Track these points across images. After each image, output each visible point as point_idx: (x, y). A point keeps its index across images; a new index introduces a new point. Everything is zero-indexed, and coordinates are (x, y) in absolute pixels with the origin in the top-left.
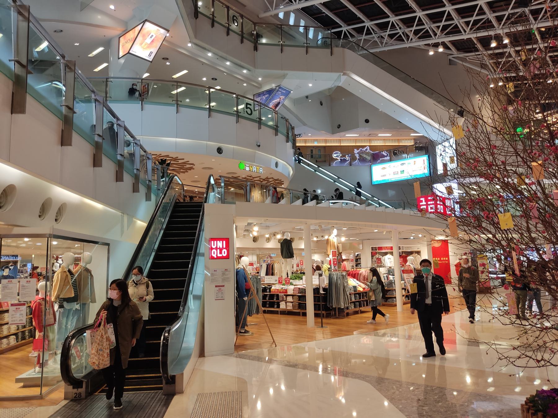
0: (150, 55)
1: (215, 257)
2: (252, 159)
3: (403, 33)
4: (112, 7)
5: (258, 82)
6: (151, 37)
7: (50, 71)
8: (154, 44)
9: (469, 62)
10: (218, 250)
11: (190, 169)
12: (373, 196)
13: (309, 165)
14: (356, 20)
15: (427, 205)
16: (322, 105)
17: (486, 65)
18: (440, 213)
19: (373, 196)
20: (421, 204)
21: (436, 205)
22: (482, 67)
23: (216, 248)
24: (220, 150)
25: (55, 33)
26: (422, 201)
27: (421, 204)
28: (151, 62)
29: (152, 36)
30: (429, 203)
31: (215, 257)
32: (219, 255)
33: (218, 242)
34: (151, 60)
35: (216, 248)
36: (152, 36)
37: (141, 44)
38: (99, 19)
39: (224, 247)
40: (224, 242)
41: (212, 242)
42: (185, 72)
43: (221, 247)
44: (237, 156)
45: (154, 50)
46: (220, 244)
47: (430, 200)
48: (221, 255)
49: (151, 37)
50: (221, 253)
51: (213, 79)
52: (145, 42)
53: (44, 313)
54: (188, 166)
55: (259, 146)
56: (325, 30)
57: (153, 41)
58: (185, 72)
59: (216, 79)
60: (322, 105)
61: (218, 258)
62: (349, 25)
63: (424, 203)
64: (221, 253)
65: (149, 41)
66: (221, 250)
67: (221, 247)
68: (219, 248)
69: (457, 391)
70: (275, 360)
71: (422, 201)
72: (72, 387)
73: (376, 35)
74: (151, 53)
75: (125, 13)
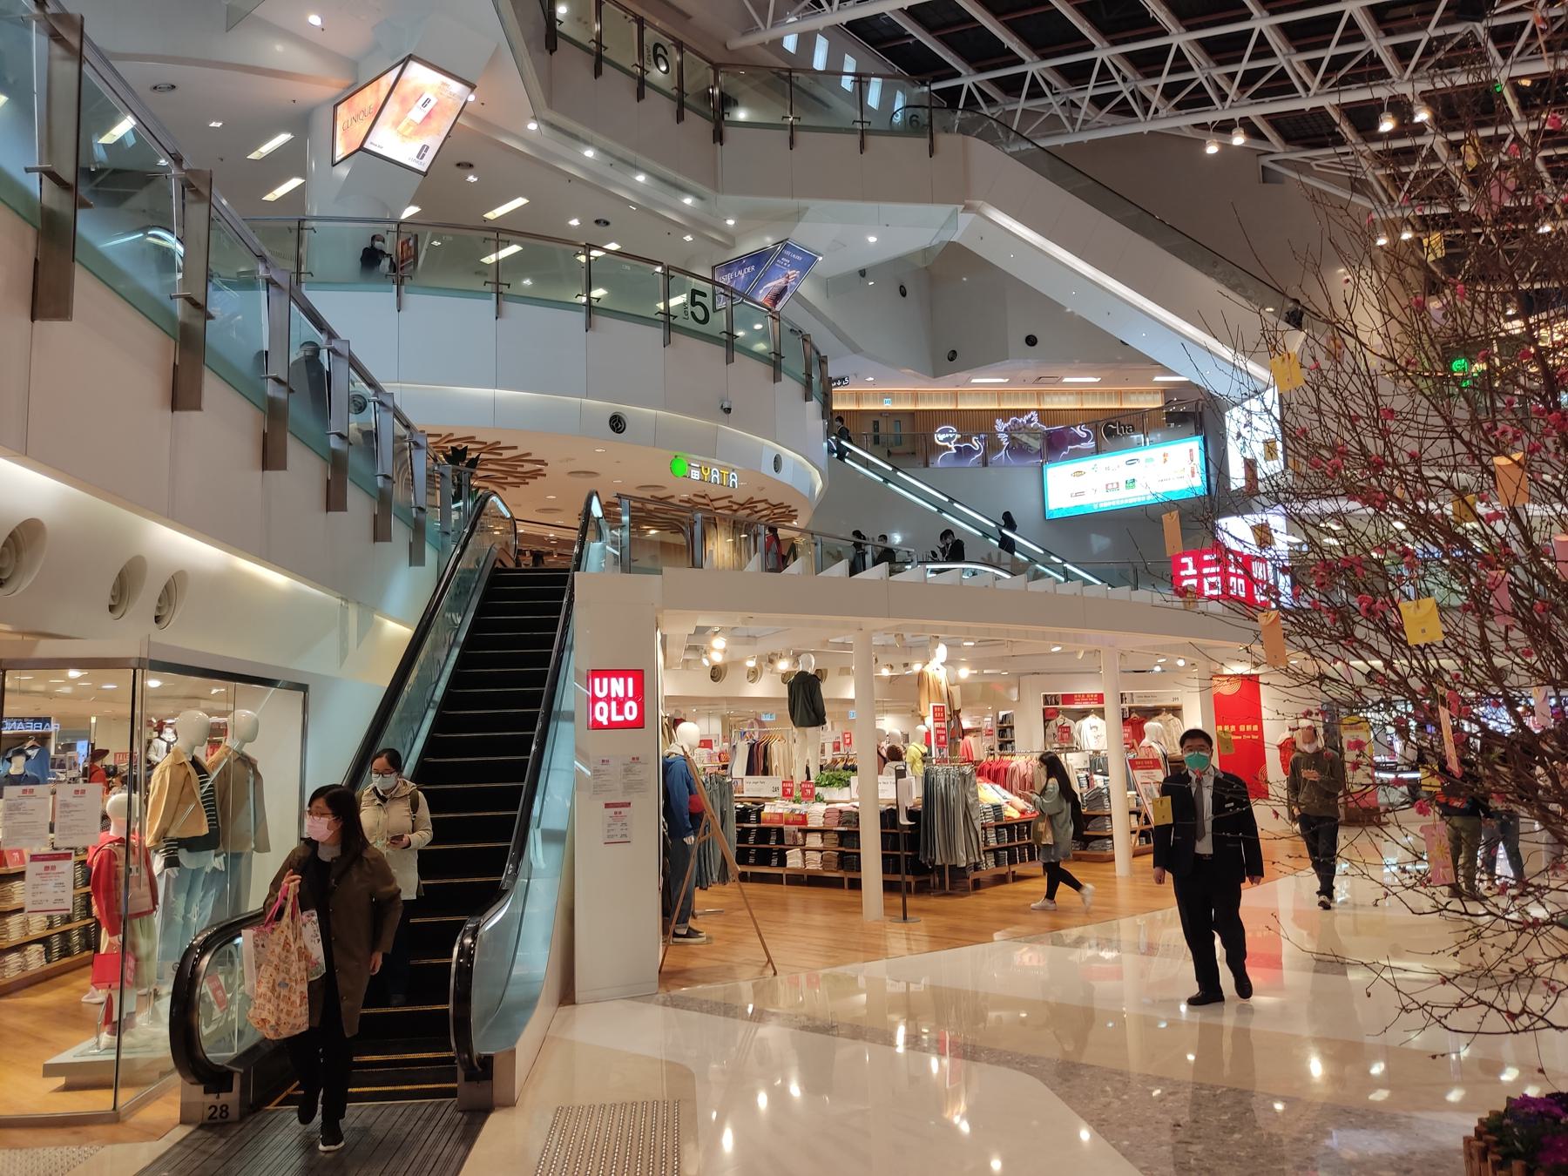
0: (421, 156)
1: (605, 723)
2: (707, 448)
3: (1132, 93)
4: (315, 20)
5: (724, 232)
6: (424, 105)
7: (141, 199)
8: (434, 124)
9: (1319, 176)
10: (614, 704)
11: (535, 474)
12: (1048, 553)
13: (867, 464)
14: (1000, 55)
15: (1200, 577)
16: (904, 294)
17: (1366, 183)
18: (1237, 598)
19: (1048, 553)
20: (1183, 573)
21: (1225, 576)
22: (1354, 189)
23: (608, 699)
24: (617, 423)
25: (156, 94)
26: (1185, 566)
27: (1183, 573)
28: (425, 174)
29: (428, 100)
30: (1206, 571)
31: (605, 723)
32: (615, 718)
33: (613, 680)
34: (424, 169)
35: (608, 699)
36: (428, 100)
37: (396, 124)
38: (279, 52)
39: (631, 694)
40: (630, 680)
41: (597, 681)
42: (520, 202)
43: (621, 695)
44: (666, 439)
45: (434, 142)
46: (617, 687)
47: (1210, 564)
48: (620, 718)
49: (424, 105)
50: (620, 711)
51: (597, 222)
52: (409, 119)
53: (123, 881)
54: (528, 467)
55: (728, 411)
56: (914, 85)
57: (429, 116)
58: (520, 202)
59: (607, 223)
60: (904, 294)
61: (612, 725)
62: (980, 70)
63: (1191, 571)
64: (620, 711)
65: (417, 114)
66: (621, 703)
67: (621, 695)
68: (617, 698)
71: (1185, 566)
72: (201, 1088)
73: (1057, 98)
74: (425, 148)
75: (351, 37)
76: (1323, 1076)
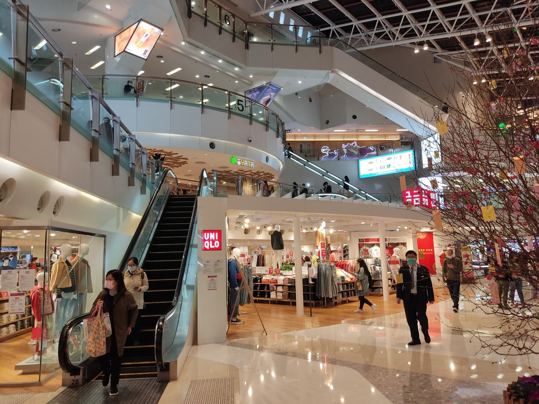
0: (145, 53)
1: (208, 248)
2: (243, 154)
3: (389, 32)
4: (108, 7)
5: (249, 80)
6: (146, 36)
7: (48, 68)
8: (149, 43)
9: (453, 60)
10: (211, 242)
11: (184, 163)
12: (360, 190)
13: (298, 159)
14: (344, 19)
16: (311, 101)
17: (469, 63)
18: (425, 206)
19: (360, 190)
20: (407, 197)
21: (421, 198)
22: (465, 65)
23: (209, 240)
24: (212, 145)
25: (53, 32)
26: (407, 195)
27: (407, 197)
28: (146, 60)
29: (147, 35)
30: (414, 196)
31: (208, 248)
32: (212, 247)
33: (211, 234)
34: (146, 58)
35: (209, 240)
36: (147, 35)
37: (136, 43)
38: (96, 18)
39: (217, 238)
40: (217, 234)
41: (205, 234)
42: (179, 69)
43: (214, 239)
44: (229, 151)
45: (149, 49)
46: (212, 236)
47: (416, 194)
48: (213, 247)
49: (146, 36)
50: (213, 244)
51: (205, 76)
52: (141, 41)
54: (181, 160)
55: (250, 141)
56: (314, 29)
57: (147, 40)
58: (179, 69)
59: (209, 77)
60: (311, 101)
61: (211, 249)
62: (337, 24)
63: (410, 196)
64: (213, 244)
65: (143, 39)
66: (213, 242)
67: (214, 239)
68: (212, 240)
69: (442, 378)
70: (266, 348)
71: (407, 195)
72: (69, 374)
73: (363, 34)
74: (146, 51)
75: (121, 13)
76: (455, 370)
